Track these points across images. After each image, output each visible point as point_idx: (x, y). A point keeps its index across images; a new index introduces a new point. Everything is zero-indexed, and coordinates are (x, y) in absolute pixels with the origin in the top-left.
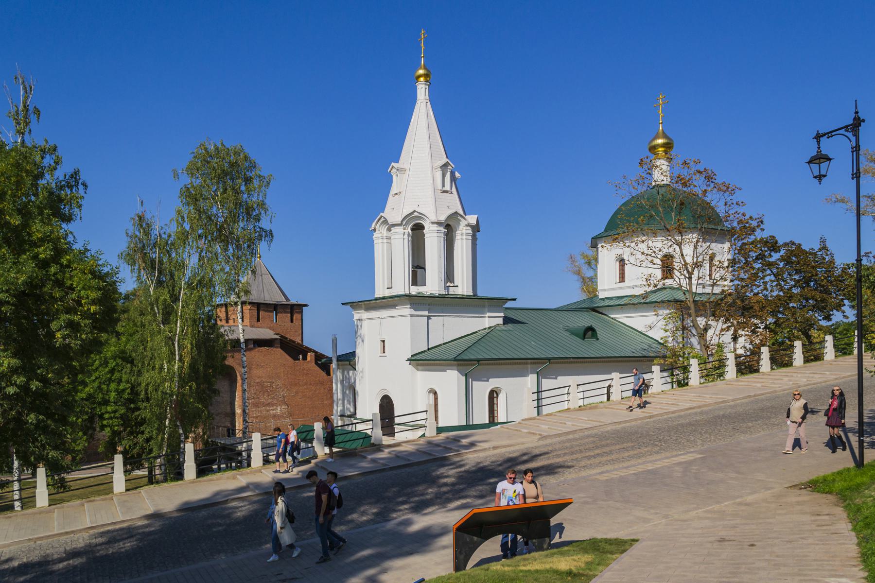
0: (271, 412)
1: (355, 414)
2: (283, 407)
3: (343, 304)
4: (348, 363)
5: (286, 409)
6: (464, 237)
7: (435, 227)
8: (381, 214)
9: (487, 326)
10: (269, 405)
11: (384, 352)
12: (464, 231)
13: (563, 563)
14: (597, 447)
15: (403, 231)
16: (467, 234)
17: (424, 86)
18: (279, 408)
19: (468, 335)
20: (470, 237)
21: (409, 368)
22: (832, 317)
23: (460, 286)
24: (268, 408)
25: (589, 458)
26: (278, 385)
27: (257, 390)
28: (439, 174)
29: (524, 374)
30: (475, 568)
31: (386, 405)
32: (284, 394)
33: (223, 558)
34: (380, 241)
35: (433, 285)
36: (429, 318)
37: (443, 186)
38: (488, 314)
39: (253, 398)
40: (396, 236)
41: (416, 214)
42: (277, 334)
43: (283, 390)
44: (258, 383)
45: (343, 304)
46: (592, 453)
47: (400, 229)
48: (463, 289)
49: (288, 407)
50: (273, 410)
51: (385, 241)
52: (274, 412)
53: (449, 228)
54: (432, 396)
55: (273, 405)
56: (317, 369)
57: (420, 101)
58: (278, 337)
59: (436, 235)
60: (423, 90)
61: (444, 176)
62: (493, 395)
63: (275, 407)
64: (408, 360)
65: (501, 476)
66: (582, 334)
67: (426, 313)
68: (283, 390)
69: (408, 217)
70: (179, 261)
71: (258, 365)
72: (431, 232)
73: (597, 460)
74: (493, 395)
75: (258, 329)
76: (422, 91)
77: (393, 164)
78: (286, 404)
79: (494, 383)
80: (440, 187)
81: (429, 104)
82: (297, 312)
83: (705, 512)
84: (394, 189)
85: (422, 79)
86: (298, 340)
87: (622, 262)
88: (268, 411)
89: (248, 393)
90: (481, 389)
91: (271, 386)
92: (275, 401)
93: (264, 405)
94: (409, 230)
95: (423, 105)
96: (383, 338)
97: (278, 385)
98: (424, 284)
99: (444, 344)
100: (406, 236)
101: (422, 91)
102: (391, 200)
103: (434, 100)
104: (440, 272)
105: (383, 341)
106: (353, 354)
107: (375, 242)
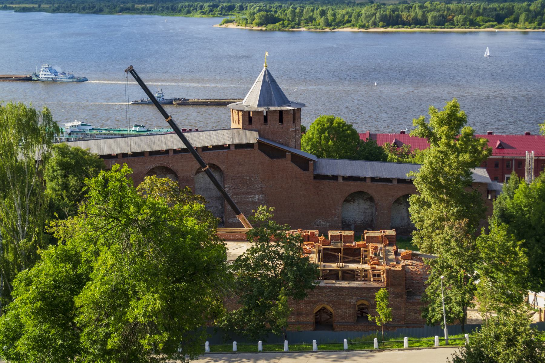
0: (250, 199)
2: (261, 196)
5: (263, 197)
10: (248, 193)
18: (257, 196)
22: (460, 114)
24: (247, 196)
26: (256, 179)
27: (237, 182)
30: (515, 147)
32: (261, 185)
33: (493, 315)
39: (234, 189)
44: (238, 177)
49: (265, 196)
50: (252, 198)
52: (253, 199)
70: (56, 103)
78: (263, 193)
83: (348, 258)
89: (44, 264)
93: (244, 193)
97: (256, 179)
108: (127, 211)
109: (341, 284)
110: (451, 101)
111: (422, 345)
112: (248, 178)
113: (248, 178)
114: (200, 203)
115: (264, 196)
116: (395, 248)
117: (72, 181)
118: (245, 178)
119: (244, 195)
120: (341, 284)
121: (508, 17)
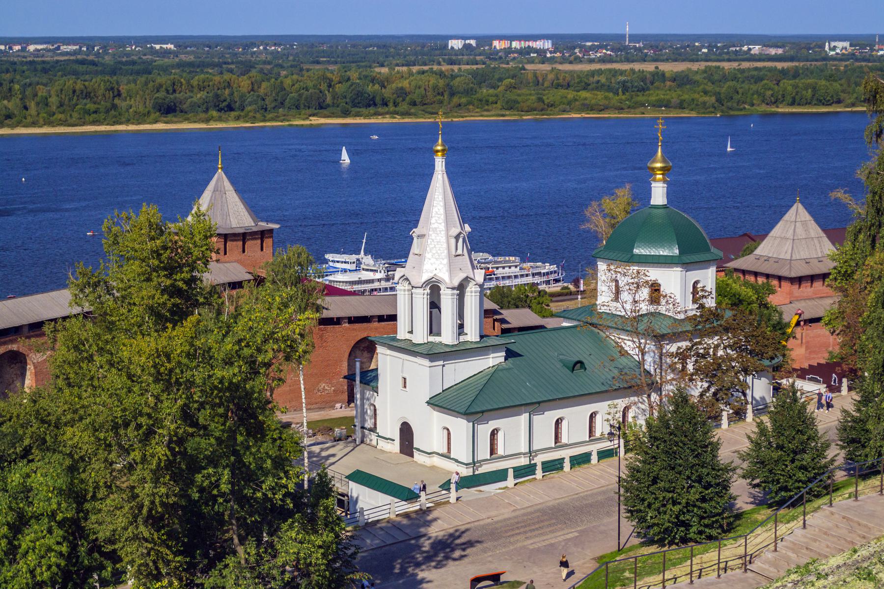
1: (375, 427)
6: (473, 294)
7: (450, 291)
9: (491, 365)
12: (473, 289)
14: (538, 522)
15: (423, 292)
16: (476, 292)
17: (441, 160)
19: (475, 375)
20: (478, 294)
21: (429, 408)
23: (469, 333)
25: (531, 531)
28: (453, 241)
29: (520, 414)
31: (406, 431)
34: (402, 293)
35: (448, 337)
36: (444, 366)
37: (457, 249)
38: (492, 355)
40: (418, 296)
41: (434, 279)
46: (533, 527)
47: (421, 291)
51: (407, 293)
53: (461, 288)
54: (446, 432)
59: (450, 297)
60: (440, 163)
61: (457, 242)
62: (494, 434)
66: (572, 366)
67: (441, 363)
69: (427, 282)
72: (446, 295)
73: (537, 532)
74: (494, 434)
75: (225, 264)
76: (440, 163)
79: (493, 424)
80: (454, 253)
81: (445, 175)
82: (267, 238)
85: (440, 154)
90: (484, 431)
94: (428, 291)
95: (440, 177)
96: (405, 376)
98: (439, 334)
99: (456, 385)
100: (425, 296)
101: (440, 163)
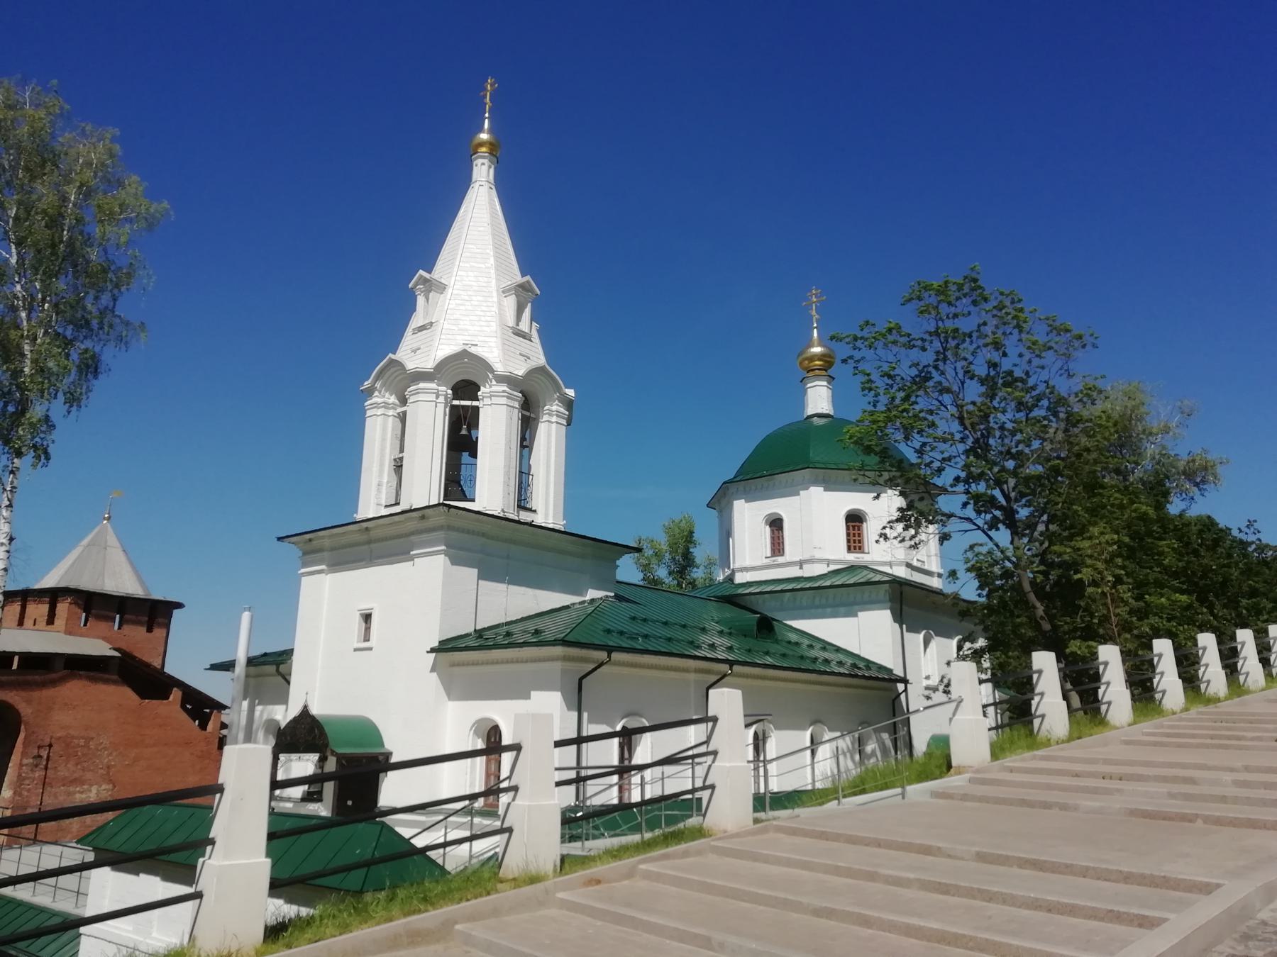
0: (78, 796)
3: (279, 539)
4: (272, 669)
5: (108, 790)
6: (554, 419)
8: (391, 355)
11: (367, 639)
13: (13, 952)
18: (94, 789)
24: (71, 789)
32: (110, 761)
42: (115, 649)
43: (110, 754)
44: (60, 738)
45: (279, 539)
48: (546, 515)
49: (115, 787)
50: (82, 793)
55: (83, 783)
56: (184, 716)
57: (478, 183)
58: (116, 654)
59: (504, 401)
63: (85, 787)
64: (433, 650)
65: (456, 923)
68: (110, 754)
71: (66, 704)
76: (483, 171)
77: (421, 272)
84: (417, 320)
86: (156, 663)
87: (776, 524)
88: (69, 794)
91: (86, 746)
92: (89, 775)
96: (365, 606)
100: (441, 399)
101: (483, 171)
102: (409, 340)
103: (506, 187)
104: (507, 474)
105: (367, 618)
106: (287, 654)
107: (369, 413)
108: (1030, 404)
109: (1171, 796)
110: (1034, 607)
111: (889, 522)
112: (82, 742)
113: (82, 742)
114: (109, 784)
115: (111, 786)
116: (1128, 570)
117: (1161, 633)
118: (76, 741)
119: (64, 785)
120: (1171, 796)
121: (1181, 588)
